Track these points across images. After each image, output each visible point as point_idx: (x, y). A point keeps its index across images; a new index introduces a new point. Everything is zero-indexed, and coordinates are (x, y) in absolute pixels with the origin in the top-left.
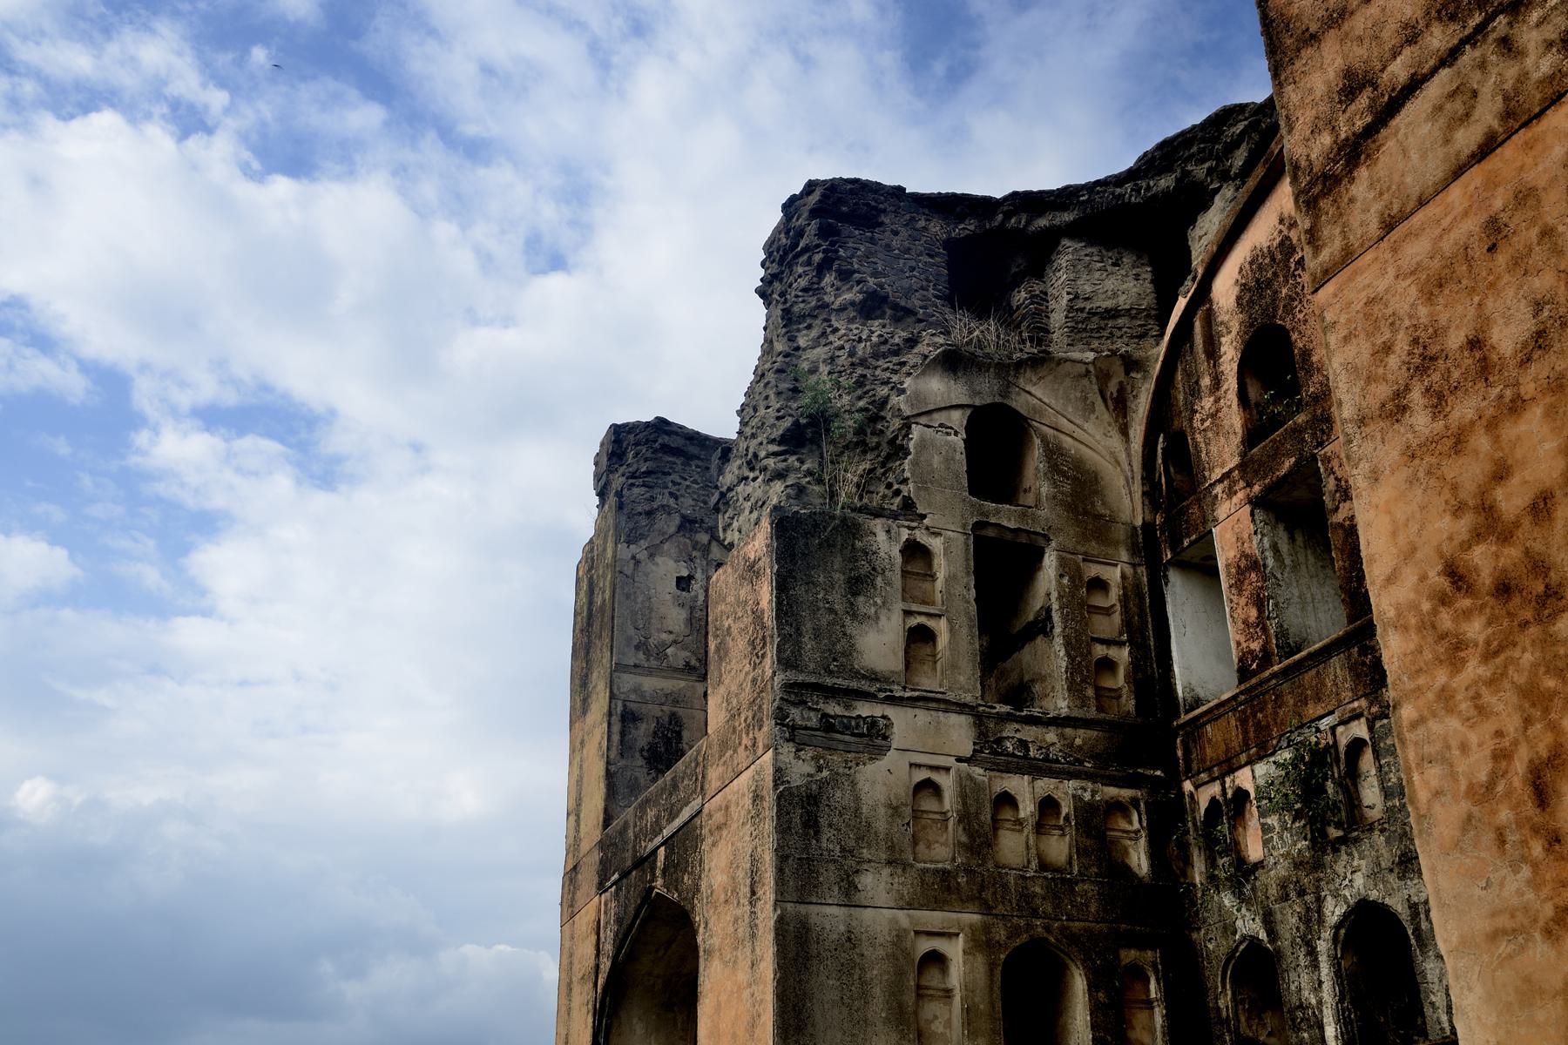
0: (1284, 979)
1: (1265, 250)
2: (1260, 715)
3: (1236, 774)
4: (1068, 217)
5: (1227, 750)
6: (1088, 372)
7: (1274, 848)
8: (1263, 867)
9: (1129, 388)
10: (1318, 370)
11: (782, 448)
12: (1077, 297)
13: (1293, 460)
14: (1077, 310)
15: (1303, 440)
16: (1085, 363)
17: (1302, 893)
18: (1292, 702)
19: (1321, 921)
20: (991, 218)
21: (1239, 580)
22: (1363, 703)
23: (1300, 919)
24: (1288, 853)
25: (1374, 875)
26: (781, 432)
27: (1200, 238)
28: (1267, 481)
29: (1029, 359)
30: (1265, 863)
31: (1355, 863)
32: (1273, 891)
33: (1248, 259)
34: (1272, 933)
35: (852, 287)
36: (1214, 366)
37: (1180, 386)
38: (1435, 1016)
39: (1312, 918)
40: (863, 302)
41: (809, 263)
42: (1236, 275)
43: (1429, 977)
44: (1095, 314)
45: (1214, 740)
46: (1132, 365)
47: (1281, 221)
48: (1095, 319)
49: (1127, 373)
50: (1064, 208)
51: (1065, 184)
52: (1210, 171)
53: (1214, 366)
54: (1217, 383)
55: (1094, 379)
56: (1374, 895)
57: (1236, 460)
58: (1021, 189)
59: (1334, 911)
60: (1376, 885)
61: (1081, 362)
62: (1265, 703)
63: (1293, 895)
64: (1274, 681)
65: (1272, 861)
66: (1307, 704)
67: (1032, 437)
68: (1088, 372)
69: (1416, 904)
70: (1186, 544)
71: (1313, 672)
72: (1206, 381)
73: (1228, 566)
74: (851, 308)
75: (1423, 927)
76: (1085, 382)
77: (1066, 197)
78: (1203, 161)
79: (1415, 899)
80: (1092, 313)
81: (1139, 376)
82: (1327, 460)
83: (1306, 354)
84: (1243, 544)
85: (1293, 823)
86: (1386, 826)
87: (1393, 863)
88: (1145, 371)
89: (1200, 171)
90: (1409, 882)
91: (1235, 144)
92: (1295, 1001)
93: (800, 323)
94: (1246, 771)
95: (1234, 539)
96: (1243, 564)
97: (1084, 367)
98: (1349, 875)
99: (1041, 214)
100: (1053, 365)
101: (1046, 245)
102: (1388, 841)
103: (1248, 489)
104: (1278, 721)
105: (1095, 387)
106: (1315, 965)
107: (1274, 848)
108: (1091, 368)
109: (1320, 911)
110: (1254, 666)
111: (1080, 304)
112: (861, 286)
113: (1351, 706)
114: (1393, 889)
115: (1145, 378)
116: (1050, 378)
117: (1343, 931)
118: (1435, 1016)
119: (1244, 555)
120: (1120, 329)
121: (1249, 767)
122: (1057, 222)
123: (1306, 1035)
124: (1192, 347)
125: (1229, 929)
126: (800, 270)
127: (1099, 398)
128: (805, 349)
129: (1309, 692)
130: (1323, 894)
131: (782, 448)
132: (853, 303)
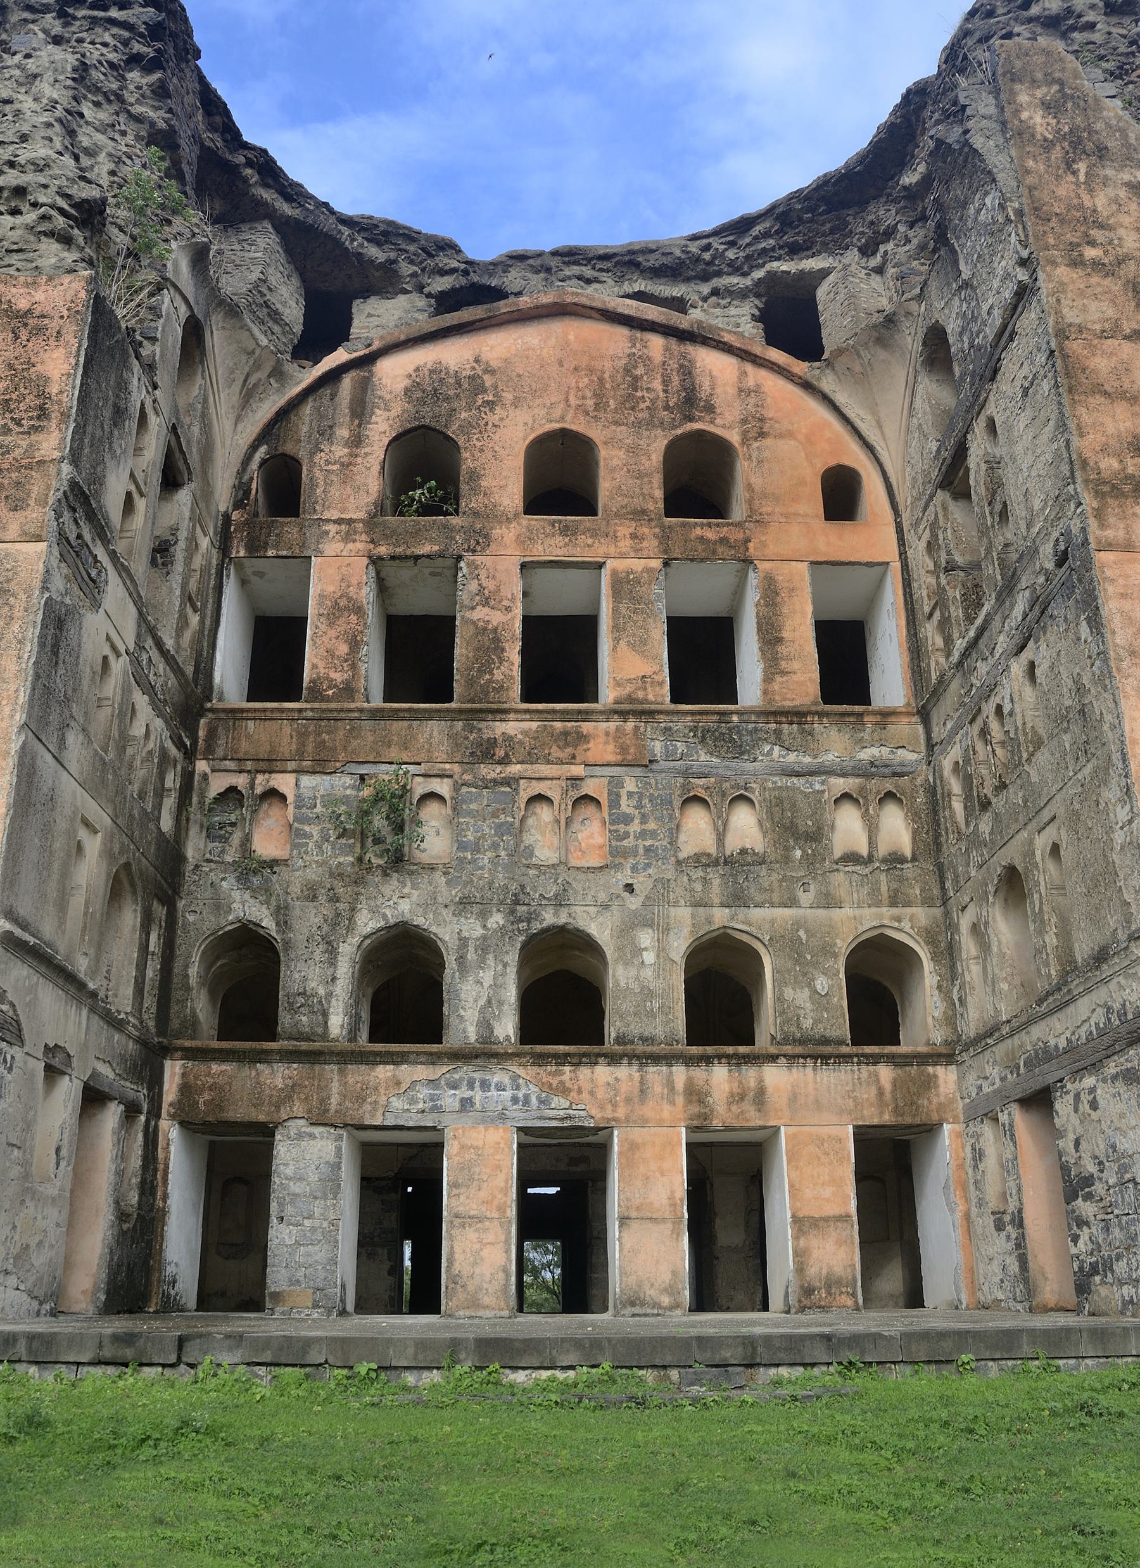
0: (289, 967)
1: (451, 372)
2: (325, 736)
3: (273, 775)
4: (286, 209)
5: (273, 749)
6: (253, 352)
7: (306, 853)
8: (287, 866)
9: (261, 389)
10: (485, 494)
11: (73, 211)
12: (265, 281)
13: (437, 548)
14: (260, 292)
15: (453, 538)
16: (257, 344)
17: (335, 899)
18: (371, 739)
19: (350, 929)
20: (233, 151)
21: (334, 614)
22: (456, 768)
23: (326, 921)
24: (324, 863)
25: (430, 903)
26: (84, 195)
27: (370, 315)
28: (398, 550)
29: (229, 305)
30: (289, 862)
31: (406, 890)
32: (296, 889)
33: (429, 366)
34: (284, 924)
35: (160, 108)
36: (359, 426)
37: (307, 419)
38: (462, 1026)
39: (341, 922)
40: (161, 131)
41: (126, 43)
42: (410, 369)
43: (463, 996)
44: (268, 307)
45: (256, 737)
46: (278, 373)
47: (477, 361)
48: (265, 310)
49: (269, 376)
50: (288, 198)
51: (300, 181)
52: (414, 275)
53: (359, 426)
54: (357, 441)
55: (251, 362)
56: (419, 921)
57: (362, 515)
58: (271, 153)
59: (367, 923)
60: (426, 913)
61: (256, 340)
62: (337, 729)
63: (322, 899)
64: (356, 715)
65: (300, 863)
66: (389, 747)
67: (195, 374)
68: (253, 352)
69: (466, 939)
70: (270, 553)
71: (406, 724)
72: (343, 432)
73: (322, 597)
74: (147, 126)
75: (469, 957)
76: (244, 358)
77: (293, 192)
78: (412, 262)
79: (465, 934)
80: (266, 304)
81: (275, 385)
82: (473, 566)
83: (474, 476)
84: (349, 586)
85: (338, 838)
86: (452, 870)
87: (452, 901)
88: (282, 385)
89: (406, 269)
90: (463, 920)
91: (443, 272)
92: (295, 988)
93: (90, 92)
94: (290, 778)
95: (338, 578)
96: (343, 602)
97: (254, 345)
98: (395, 899)
99: (266, 186)
100: (238, 325)
101: (260, 212)
102: (448, 883)
103: (372, 546)
104: (349, 749)
105: (247, 369)
106: (332, 962)
107: (306, 853)
108: (258, 352)
109: (351, 919)
110: (330, 692)
111: (264, 290)
112: (169, 116)
113: (442, 766)
114: (445, 921)
115: (278, 390)
116: (228, 333)
117: (368, 941)
118: (462, 1026)
119: (345, 595)
120: (273, 333)
121: (294, 775)
122: (277, 205)
123: (304, 1019)
124: (333, 396)
125: (219, 905)
126: (107, 38)
127: (242, 380)
128: (87, 123)
129: (395, 738)
130: (359, 906)
131: (73, 211)
132: (152, 124)
